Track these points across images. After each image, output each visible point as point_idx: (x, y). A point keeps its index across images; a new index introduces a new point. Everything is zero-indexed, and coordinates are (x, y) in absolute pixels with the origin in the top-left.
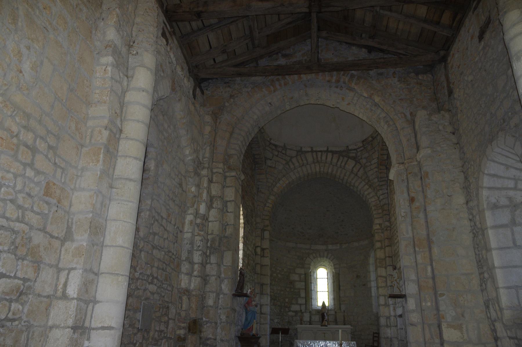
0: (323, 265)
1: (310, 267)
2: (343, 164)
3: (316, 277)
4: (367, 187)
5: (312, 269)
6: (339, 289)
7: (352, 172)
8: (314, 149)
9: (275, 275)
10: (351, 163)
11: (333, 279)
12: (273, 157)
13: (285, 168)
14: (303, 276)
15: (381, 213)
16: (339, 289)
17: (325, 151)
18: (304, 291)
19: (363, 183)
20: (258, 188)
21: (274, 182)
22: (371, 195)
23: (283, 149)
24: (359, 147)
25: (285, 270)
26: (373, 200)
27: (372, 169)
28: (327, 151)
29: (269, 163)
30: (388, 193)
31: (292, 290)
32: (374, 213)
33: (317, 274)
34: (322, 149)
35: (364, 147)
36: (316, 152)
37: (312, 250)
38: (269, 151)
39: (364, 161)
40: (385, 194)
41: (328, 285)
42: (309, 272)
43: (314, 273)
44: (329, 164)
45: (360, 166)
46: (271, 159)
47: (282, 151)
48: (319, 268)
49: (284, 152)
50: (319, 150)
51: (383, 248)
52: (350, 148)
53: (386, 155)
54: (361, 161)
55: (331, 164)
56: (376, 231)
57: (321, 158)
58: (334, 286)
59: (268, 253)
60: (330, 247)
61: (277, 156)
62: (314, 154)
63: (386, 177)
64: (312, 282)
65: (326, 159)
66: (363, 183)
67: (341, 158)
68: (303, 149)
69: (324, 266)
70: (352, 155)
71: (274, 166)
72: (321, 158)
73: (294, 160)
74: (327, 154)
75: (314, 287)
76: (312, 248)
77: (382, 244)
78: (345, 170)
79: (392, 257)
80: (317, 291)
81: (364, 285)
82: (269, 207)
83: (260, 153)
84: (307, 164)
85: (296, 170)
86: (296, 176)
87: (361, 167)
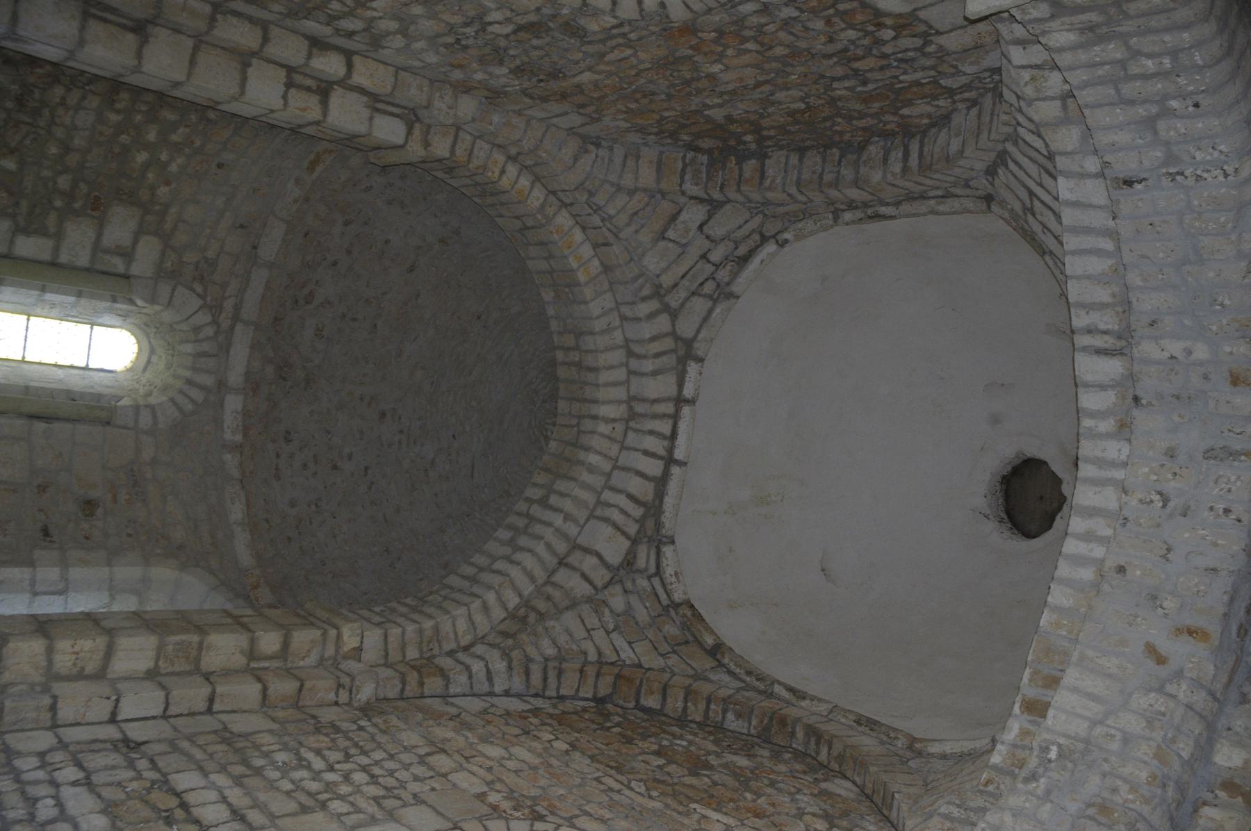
0: (155, 359)
1: (158, 304)
2: (616, 516)
3: (100, 321)
4: (513, 601)
5: (145, 311)
6: (32, 417)
7: (575, 547)
8: (686, 410)
9: (152, 136)
10: (614, 550)
11: (83, 395)
12: (708, 237)
13: (640, 281)
14: (119, 265)
15: (404, 657)
16: (32, 417)
17: (670, 450)
18: (46, 256)
19: (528, 589)
20: (598, 145)
21: (603, 220)
22: (479, 618)
23: (718, 285)
24: (669, 587)
25: (163, 191)
26: (462, 625)
27: (592, 632)
28: (670, 460)
29: (693, 215)
30: (491, 694)
31: (58, 203)
32: (410, 628)
33: (109, 329)
34: (681, 440)
35: (668, 606)
36: (675, 417)
37: (232, 328)
38: (740, 227)
39: (618, 603)
40: (487, 684)
41: (56, 365)
42: (133, 297)
43: (125, 316)
44: (617, 461)
45: (600, 584)
46: (705, 228)
47: (714, 279)
48: (138, 342)
49: (709, 287)
50: (683, 427)
51: (254, 665)
52: (667, 550)
53: (659, 707)
54: (618, 588)
55: (615, 467)
56: (333, 633)
57: (651, 432)
58: (52, 393)
59: (304, 110)
60: (233, 403)
61: (704, 257)
62: (669, 408)
63: (558, 692)
64: (83, 301)
65: (646, 453)
66: (528, 589)
67: (638, 512)
68: (693, 364)
69: (149, 362)
70: (644, 557)
71: (671, 234)
72: (651, 432)
73: (663, 323)
74: (661, 458)
75: (53, 305)
76: (239, 327)
77: (271, 658)
78: (588, 520)
79: (209, 711)
80: (29, 315)
81: (46, 532)
82: (503, 172)
83: (767, 182)
84: (631, 373)
85: (617, 323)
86: (598, 317)
87: (595, 588)
